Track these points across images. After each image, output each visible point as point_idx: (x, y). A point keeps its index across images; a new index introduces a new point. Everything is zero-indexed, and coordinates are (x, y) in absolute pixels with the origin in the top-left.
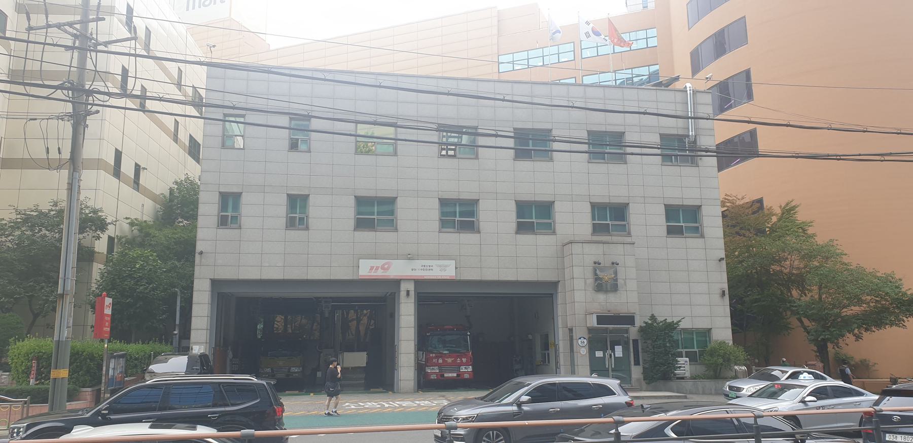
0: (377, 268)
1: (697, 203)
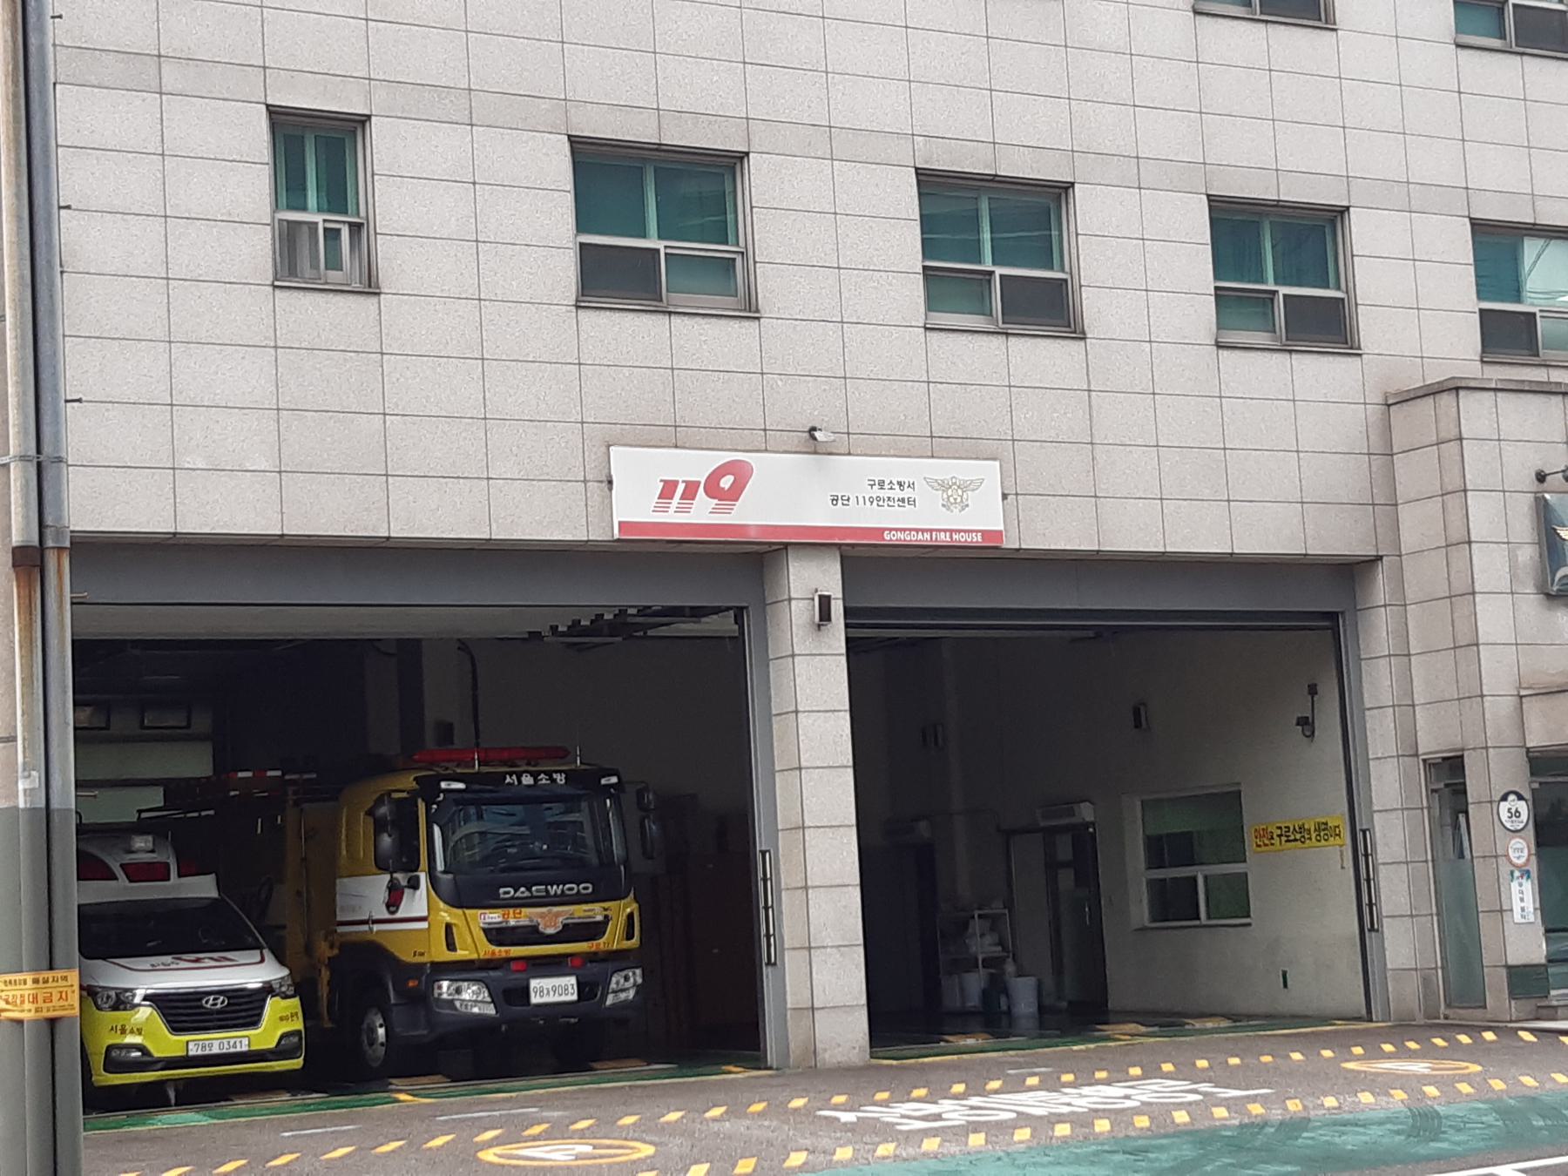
0: (691, 490)
1: (352, 105)
